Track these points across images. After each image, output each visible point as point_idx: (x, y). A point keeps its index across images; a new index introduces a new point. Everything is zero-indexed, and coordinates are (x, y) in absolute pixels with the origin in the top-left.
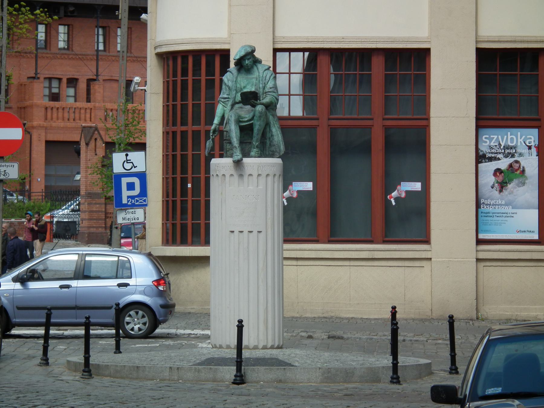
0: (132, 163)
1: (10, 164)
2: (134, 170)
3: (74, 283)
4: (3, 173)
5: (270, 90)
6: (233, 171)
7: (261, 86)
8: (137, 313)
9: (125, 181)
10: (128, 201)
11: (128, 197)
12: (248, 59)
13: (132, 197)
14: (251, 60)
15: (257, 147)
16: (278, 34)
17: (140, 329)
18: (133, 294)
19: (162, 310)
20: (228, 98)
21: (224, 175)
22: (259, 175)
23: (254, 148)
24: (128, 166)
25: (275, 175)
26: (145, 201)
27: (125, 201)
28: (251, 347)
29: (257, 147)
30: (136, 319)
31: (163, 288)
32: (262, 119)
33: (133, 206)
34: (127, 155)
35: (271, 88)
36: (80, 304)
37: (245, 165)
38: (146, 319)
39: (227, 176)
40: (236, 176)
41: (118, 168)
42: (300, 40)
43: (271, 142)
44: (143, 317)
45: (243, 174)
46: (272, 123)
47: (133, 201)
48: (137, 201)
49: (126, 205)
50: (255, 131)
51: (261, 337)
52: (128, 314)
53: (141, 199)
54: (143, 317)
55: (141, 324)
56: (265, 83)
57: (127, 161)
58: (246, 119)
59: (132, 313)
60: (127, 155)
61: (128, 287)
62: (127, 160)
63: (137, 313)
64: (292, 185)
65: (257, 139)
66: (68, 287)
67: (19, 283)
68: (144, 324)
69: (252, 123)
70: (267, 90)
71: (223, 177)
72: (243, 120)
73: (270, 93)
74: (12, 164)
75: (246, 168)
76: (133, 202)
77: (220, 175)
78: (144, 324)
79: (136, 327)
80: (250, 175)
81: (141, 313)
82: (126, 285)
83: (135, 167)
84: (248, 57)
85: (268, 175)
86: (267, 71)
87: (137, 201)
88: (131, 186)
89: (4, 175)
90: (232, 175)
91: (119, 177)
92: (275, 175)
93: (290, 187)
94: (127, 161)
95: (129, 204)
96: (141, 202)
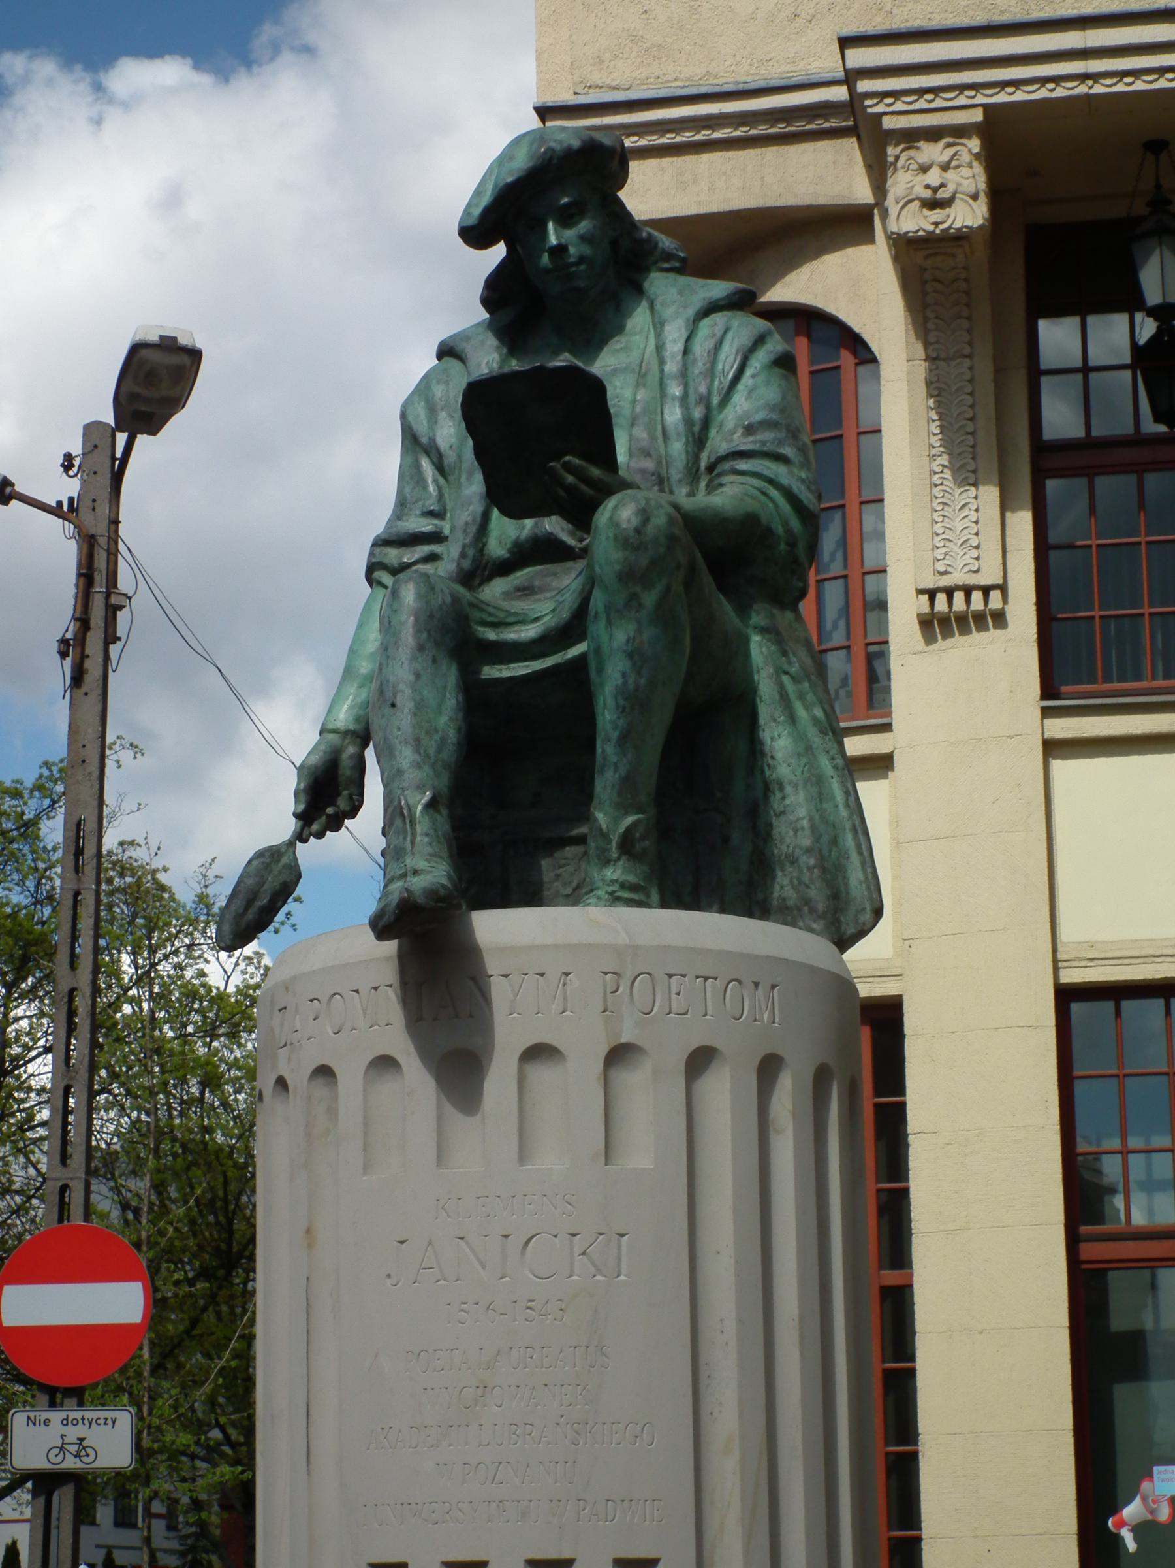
1: (102, 1414)
4: (74, 1449)
5: (747, 444)
6: (395, 1038)
7: (673, 415)
12: (566, 218)
14: (584, 226)
15: (627, 845)
16: (1066, 934)
20: (436, 537)
21: (324, 1072)
22: (619, 1055)
23: (606, 862)
25: (769, 1069)
29: (627, 845)
32: (650, 598)
35: (749, 430)
37: (493, 966)
39: (350, 1075)
40: (417, 1077)
42: (1152, 952)
46: (766, 687)
50: (607, 716)
58: (529, 632)
64: (1150, 1476)
65: (628, 784)
69: (582, 658)
70: (718, 444)
71: (320, 1085)
72: (511, 635)
73: (742, 465)
74: (109, 1415)
75: (499, 991)
77: (298, 1079)
86: (719, 320)
89: (78, 1456)
90: (385, 1063)
92: (769, 1069)
93: (1145, 1486)
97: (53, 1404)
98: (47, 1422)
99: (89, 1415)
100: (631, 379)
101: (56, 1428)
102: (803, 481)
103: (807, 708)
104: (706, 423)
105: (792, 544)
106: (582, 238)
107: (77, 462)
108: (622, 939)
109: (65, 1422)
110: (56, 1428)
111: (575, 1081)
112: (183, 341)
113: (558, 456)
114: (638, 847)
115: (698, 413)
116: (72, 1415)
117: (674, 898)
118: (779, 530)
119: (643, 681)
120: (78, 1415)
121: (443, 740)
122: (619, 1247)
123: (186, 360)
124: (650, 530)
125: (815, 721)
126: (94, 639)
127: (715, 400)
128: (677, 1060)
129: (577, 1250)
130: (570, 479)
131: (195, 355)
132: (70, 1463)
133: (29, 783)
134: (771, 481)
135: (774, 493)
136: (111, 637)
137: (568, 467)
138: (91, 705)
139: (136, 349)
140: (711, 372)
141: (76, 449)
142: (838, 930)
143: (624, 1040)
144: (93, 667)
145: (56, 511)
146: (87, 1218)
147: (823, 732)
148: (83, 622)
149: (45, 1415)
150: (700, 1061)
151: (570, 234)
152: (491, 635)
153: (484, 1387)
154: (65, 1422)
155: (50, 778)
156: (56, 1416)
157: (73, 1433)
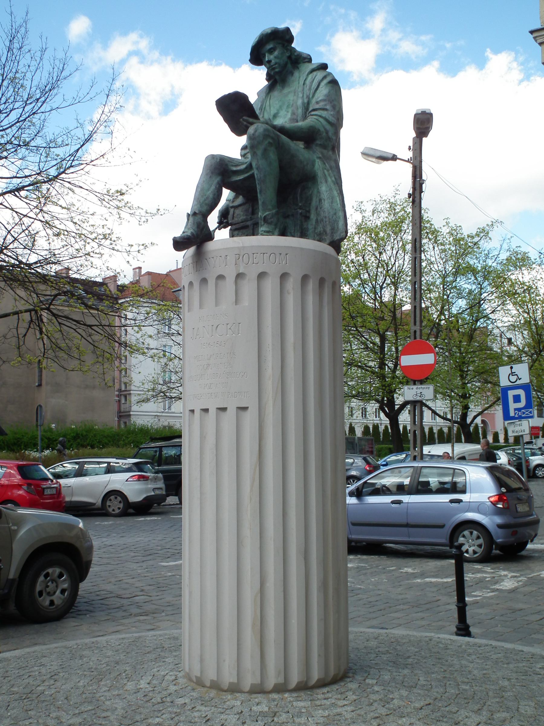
0: (516, 375)
2: (519, 382)
3: (406, 499)
4: (419, 395)
5: (317, 106)
7: (300, 102)
8: (471, 533)
9: (511, 394)
10: (515, 414)
11: (515, 409)
13: (519, 410)
14: (276, 53)
17: (475, 552)
18: (467, 512)
19: (500, 531)
22: (239, 276)
24: (513, 378)
25: (284, 276)
26: (531, 412)
27: (512, 414)
28: (225, 686)
30: (470, 541)
31: (503, 505)
33: (520, 418)
34: (512, 368)
36: (411, 521)
38: (481, 541)
41: (504, 382)
43: (318, 214)
44: (478, 538)
45: (206, 276)
47: (520, 413)
48: (524, 413)
49: (513, 418)
51: (250, 663)
52: (461, 535)
53: (527, 411)
54: (478, 538)
55: (476, 547)
56: (308, 97)
57: (512, 374)
59: (466, 533)
60: (512, 368)
61: (461, 503)
62: (512, 373)
63: (471, 533)
66: (399, 502)
67: (355, 498)
68: (480, 546)
72: (239, 168)
76: (520, 414)
78: (480, 546)
79: (471, 550)
80: (221, 277)
81: (475, 533)
82: (459, 501)
83: (520, 379)
84: (269, 46)
85: (262, 276)
87: (524, 413)
88: (517, 399)
91: (505, 390)
92: (284, 276)
94: (512, 374)
95: (516, 416)
96: (527, 414)
97: (415, 384)
98: (412, 389)
99: (422, 386)
100: (293, 94)
101: (415, 390)
102: (331, 115)
103: (331, 178)
104: (308, 103)
105: (327, 132)
106: (275, 57)
107: (412, 148)
108: (241, 245)
109: (417, 388)
110: (415, 390)
111: (229, 284)
112: (427, 112)
113: (242, 117)
114: (270, 221)
115: (306, 101)
116: (419, 387)
117: (283, 233)
118: (322, 129)
119: (262, 176)
120: (420, 387)
121: (207, 198)
122: (239, 326)
123: (429, 116)
124: (257, 134)
125: (333, 181)
126: (417, 192)
127: (311, 96)
128: (255, 275)
129: (229, 328)
130: (245, 123)
131: (431, 115)
132: (418, 398)
133: (474, 233)
134: (320, 116)
135: (321, 119)
136: (421, 191)
137: (244, 120)
138: (417, 209)
139: (415, 115)
140: (310, 89)
141: (411, 145)
142: (333, 236)
143: (240, 272)
144: (417, 200)
145: (408, 161)
146: (421, 338)
147: (334, 184)
148: (414, 188)
149: (412, 387)
150: (262, 276)
151: (272, 57)
152: (234, 169)
153: (209, 365)
154: (417, 388)
155: (480, 232)
156: (415, 387)
157: (419, 391)
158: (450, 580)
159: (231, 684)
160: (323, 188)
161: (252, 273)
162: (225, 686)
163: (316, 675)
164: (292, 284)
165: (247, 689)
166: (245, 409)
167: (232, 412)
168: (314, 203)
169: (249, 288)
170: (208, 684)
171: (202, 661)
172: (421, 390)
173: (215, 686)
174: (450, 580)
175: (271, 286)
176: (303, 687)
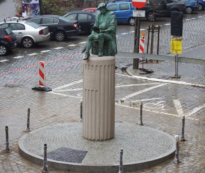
25: (105, 66)
28: (92, 140)
51: (97, 134)
101: (137, 12)
109: (138, 12)
110: (137, 12)
111: (95, 68)
150: (101, 66)
154: (138, 12)
157: (139, 13)
158: (169, 24)
159: (94, 139)
160: (113, 43)
161: (99, 66)
162: (92, 140)
163: (109, 138)
164: (106, 67)
165: (96, 140)
166: (97, 91)
167: (94, 91)
168: (110, 45)
169: (98, 68)
170: (89, 139)
171: (88, 135)
172: (140, 13)
173: (90, 140)
174: (169, 24)
175: (102, 68)
176: (106, 140)
